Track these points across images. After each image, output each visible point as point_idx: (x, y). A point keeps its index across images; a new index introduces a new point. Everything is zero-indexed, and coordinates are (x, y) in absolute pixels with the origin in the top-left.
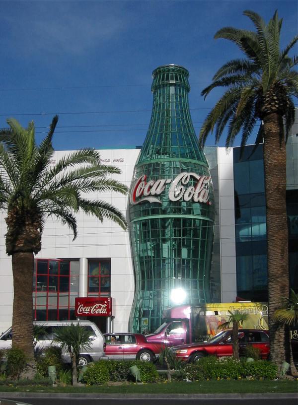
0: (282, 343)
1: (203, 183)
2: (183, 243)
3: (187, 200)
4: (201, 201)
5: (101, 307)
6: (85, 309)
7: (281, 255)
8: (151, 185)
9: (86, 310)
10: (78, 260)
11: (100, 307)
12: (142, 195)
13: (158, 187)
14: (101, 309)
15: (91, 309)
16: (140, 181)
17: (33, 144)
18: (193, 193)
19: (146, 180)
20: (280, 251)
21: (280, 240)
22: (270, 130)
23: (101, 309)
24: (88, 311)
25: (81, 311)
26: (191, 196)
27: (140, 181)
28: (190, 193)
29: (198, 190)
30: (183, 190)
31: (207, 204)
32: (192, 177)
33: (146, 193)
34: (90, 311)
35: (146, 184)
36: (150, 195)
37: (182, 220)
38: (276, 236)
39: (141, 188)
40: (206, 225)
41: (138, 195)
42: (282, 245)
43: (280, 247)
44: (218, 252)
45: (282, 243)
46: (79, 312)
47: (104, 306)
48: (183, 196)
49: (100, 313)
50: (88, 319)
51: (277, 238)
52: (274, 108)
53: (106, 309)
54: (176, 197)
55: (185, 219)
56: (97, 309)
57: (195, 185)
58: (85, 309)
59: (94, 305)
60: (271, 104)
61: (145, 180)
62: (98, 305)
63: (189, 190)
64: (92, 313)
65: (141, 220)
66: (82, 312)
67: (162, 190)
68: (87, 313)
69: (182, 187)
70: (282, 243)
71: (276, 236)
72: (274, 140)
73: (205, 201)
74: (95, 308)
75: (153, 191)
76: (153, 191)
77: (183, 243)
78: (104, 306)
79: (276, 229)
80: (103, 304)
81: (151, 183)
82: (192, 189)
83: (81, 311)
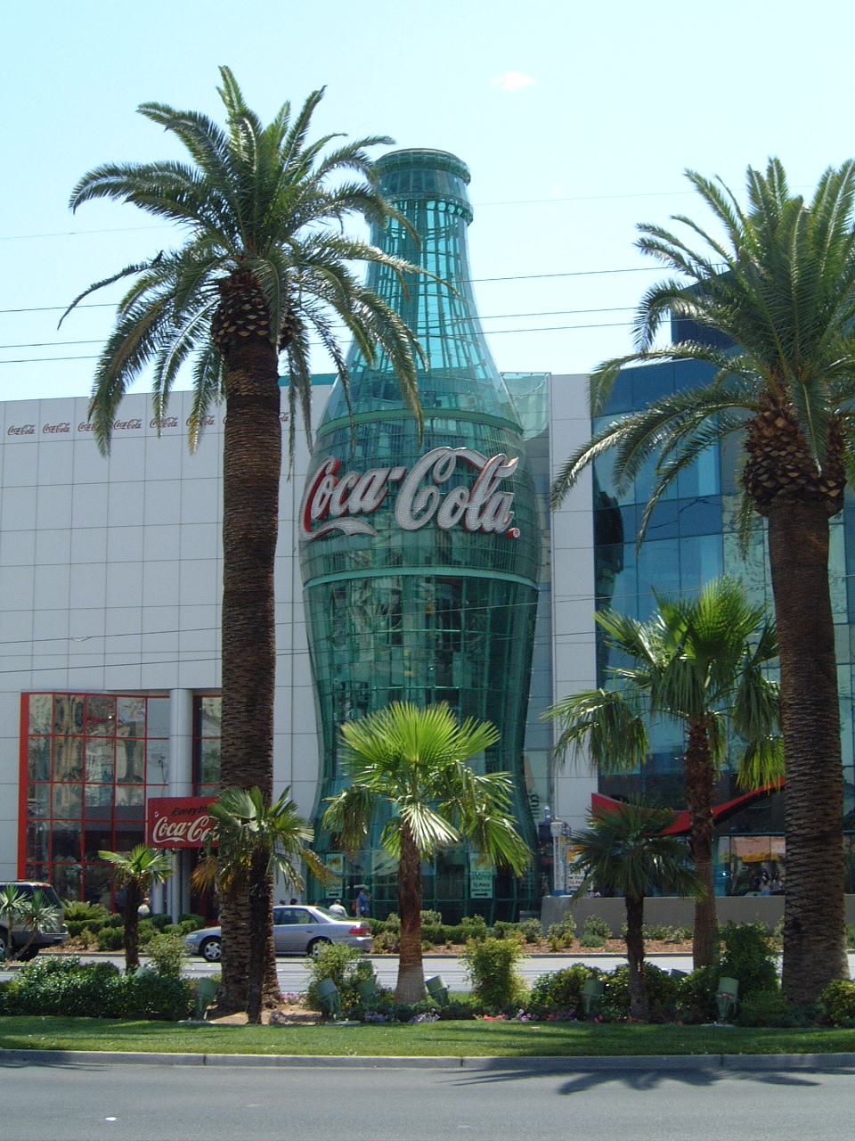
1: (494, 478)
4: (488, 527)
6: (173, 830)
7: (247, 711)
8: (350, 486)
9: (175, 833)
10: (165, 694)
12: (325, 516)
13: (498, 508)
15: (188, 828)
16: (323, 475)
17: (741, 216)
18: (463, 506)
19: (339, 472)
20: (244, 700)
21: (246, 670)
22: (237, 390)
24: (181, 833)
25: (161, 834)
27: (323, 475)
28: (455, 509)
29: (479, 498)
30: (436, 500)
31: (508, 535)
32: (461, 461)
33: (336, 509)
35: (336, 484)
36: (346, 514)
37: (464, 584)
38: (237, 660)
39: (324, 496)
41: (317, 511)
42: (251, 684)
43: (244, 691)
45: (252, 680)
46: (158, 838)
48: (437, 512)
51: (238, 667)
52: (244, 334)
54: (418, 517)
55: (471, 580)
56: (204, 829)
57: (472, 487)
58: (173, 830)
60: (236, 324)
61: (334, 473)
63: (454, 497)
64: (191, 840)
66: (165, 836)
67: (378, 500)
68: (176, 840)
69: (433, 489)
70: (252, 680)
71: (237, 660)
72: (243, 414)
73: (500, 525)
75: (355, 503)
76: (355, 503)
79: (237, 644)
81: (349, 479)
82: (462, 496)
83: (161, 834)
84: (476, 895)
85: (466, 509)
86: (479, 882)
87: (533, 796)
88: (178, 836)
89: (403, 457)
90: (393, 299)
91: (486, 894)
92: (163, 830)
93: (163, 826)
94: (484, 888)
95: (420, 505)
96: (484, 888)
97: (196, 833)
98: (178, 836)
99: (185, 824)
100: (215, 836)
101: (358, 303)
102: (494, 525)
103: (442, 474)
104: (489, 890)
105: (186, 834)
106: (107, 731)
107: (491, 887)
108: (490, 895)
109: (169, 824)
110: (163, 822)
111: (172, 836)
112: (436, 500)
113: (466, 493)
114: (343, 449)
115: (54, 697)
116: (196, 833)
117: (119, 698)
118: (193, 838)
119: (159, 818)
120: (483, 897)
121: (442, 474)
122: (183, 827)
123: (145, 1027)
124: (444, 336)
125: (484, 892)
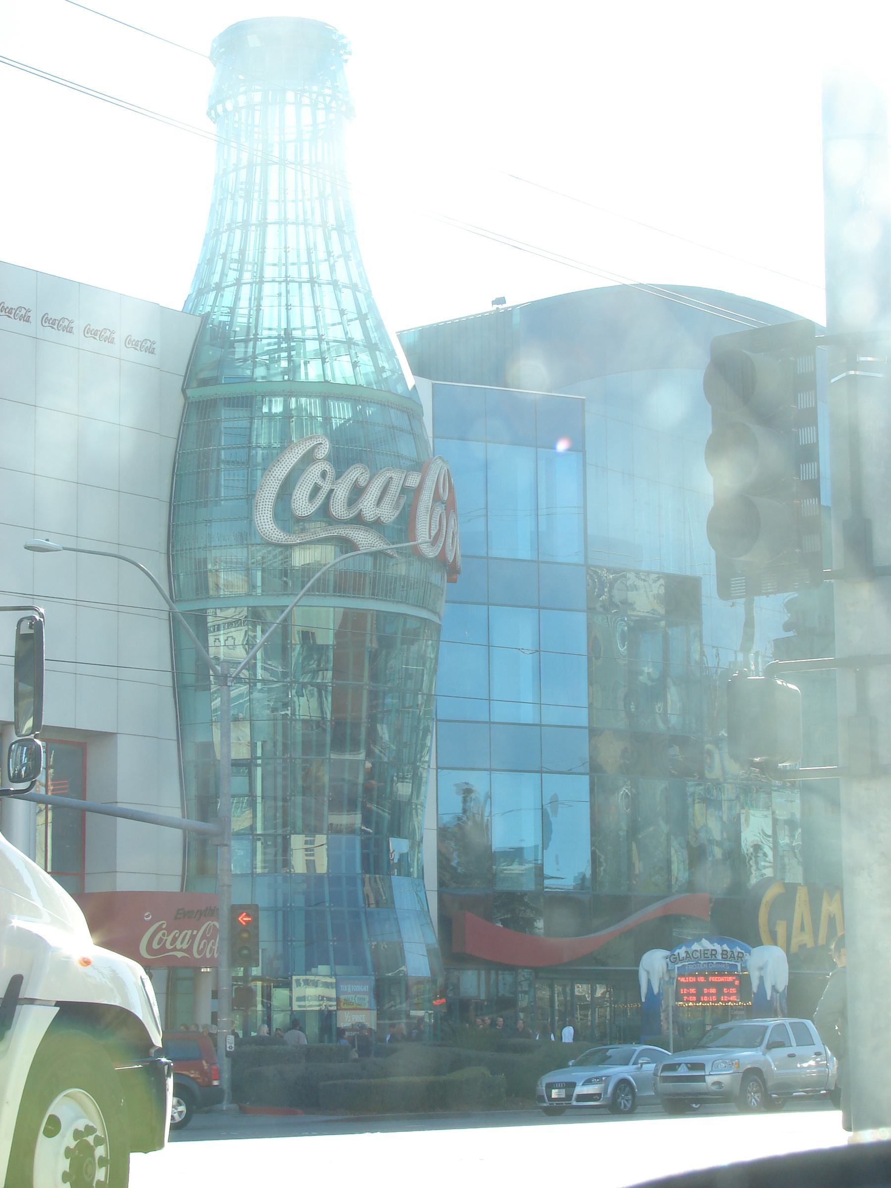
6: (174, 940)
9: (178, 945)
15: (193, 937)
24: (185, 946)
25: (155, 946)
28: (316, 489)
36: (358, 520)
58: (174, 940)
66: (163, 949)
68: (179, 954)
82: (324, 475)
85: (332, 491)
88: (181, 950)
89: (178, 505)
90: (238, 232)
92: (161, 940)
93: (160, 935)
97: (201, 946)
98: (181, 950)
99: (189, 932)
102: (378, 511)
106: (242, 183)
109: (169, 930)
110: (159, 929)
111: (175, 949)
114: (246, 347)
115: (334, 610)
116: (201, 946)
117: (303, 284)
119: (152, 923)
122: (188, 937)
124: (324, 224)
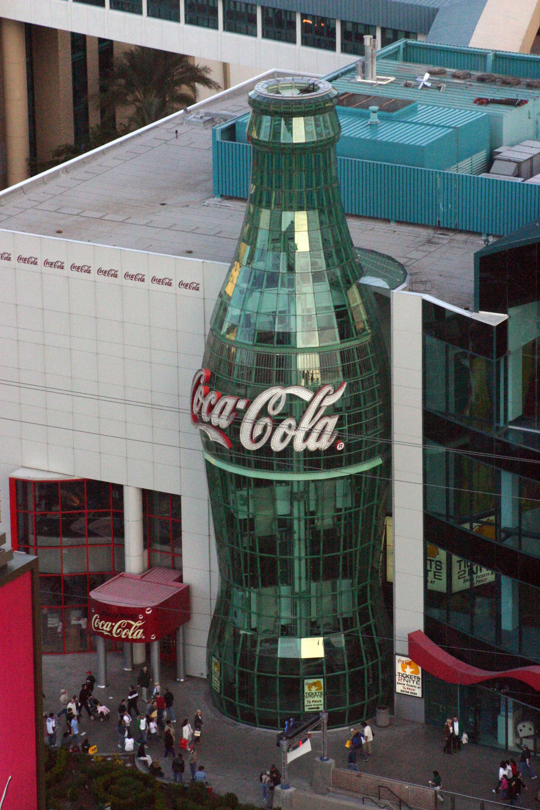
0: (251, 421)
2: (438, 569)
3: (388, 722)
5: (132, 625)
6: (103, 625)
9: (104, 627)
11: (129, 626)
14: (131, 631)
15: (112, 627)
18: (291, 433)
23: (131, 631)
24: (108, 629)
26: (288, 440)
28: (285, 436)
29: (306, 424)
30: (269, 429)
34: (111, 632)
40: (376, 415)
44: (523, 398)
47: (138, 624)
49: (130, 637)
50: (522, 44)
53: (142, 631)
56: (124, 629)
58: (103, 625)
59: (120, 620)
62: (126, 621)
63: (125, 631)
64: (115, 635)
65: (355, 340)
68: (106, 633)
73: (324, 444)
74: (119, 627)
77: (438, 569)
78: (138, 624)
80: (136, 620)
82: (290, 426)
84: (309, 709)
86: (311, 699)
87: (437, 561)
91: (318, 708)
92: (97, 624)
94: (316, 703)
95: (258, 432)
96: (316, 703)
98: (106, 631)
100: (148, 611)
101: (61, 492)
103: (274, 409)
104: (321, 705)
105: (111, 630)
107: (322, 702)
108: (321, 708)
110: (96, 618)
112: (269, 429)
113: (293, 422)
118: (117, 634)
120: (316, 710)
121: (274, 409)
123: (184, 633)
125: (316, 707)
